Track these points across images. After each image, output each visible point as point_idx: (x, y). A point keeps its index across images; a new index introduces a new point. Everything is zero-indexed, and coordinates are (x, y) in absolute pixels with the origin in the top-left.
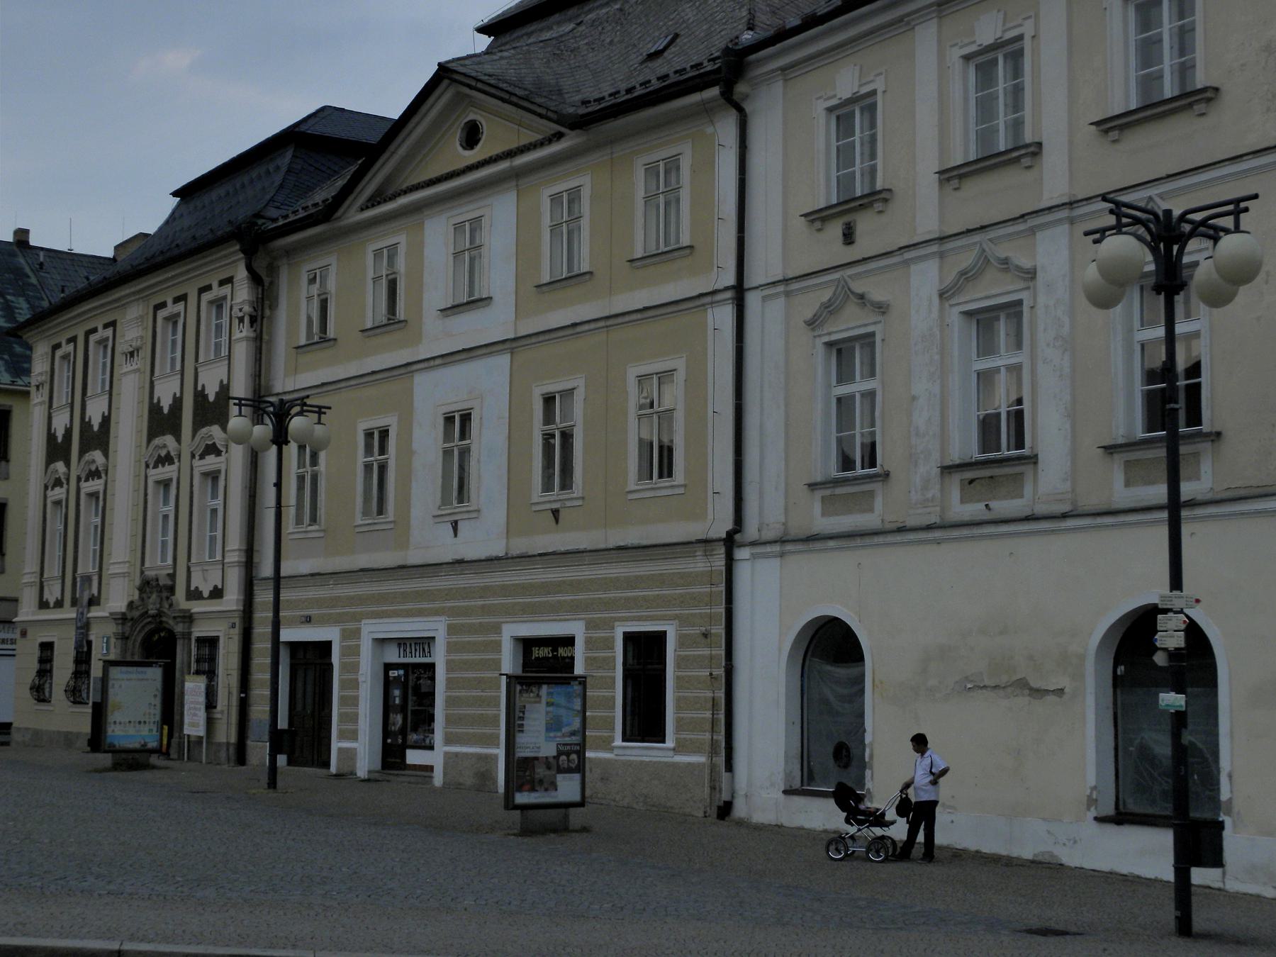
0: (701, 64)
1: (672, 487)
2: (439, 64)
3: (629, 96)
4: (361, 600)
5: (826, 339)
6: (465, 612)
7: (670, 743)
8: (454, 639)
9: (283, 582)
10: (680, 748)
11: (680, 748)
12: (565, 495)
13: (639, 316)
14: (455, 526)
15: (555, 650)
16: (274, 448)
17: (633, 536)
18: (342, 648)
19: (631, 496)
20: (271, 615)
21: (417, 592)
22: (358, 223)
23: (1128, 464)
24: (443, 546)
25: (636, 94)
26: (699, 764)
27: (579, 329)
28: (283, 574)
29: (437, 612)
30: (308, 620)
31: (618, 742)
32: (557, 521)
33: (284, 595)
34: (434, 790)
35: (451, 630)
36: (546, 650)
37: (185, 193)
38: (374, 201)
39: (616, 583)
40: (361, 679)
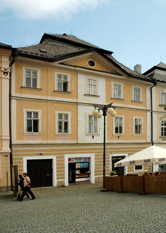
0: (134, 75)
1: (97, 134)
2: (45, 34)
3: (141, 77)
4: (64, 150)
5: (162, 120)
6: (97, 152)
7: (143, 169)
8: (97, 157)
9: (106, 144)
10: (144, 169)
11: (144, 169)
12: (120, 134)
13: (136, 110)
14: (93, 136)
15: (117, 158)
16: (103, 117)
17: (49, 142)
18: (57, 161)
19: (134, 136)
20: (103, 151)
21: (85, 149)
22: (56, 66)
23: (162, 139)
24: (89, 140)
25: (38, 56)
26: (147, 171)
27: (124, 108)
28: (13, 143)
29: (93, 152)
30: (41, 154)
31: (134, 170)
32: (118, 138)
33: (106, 147)
34: (93, 184)
35: (57, 158)
36: (115, 158)
37: (46, 37)
38: (60, 64)
39: (134, 148)
40: (65, 166)
